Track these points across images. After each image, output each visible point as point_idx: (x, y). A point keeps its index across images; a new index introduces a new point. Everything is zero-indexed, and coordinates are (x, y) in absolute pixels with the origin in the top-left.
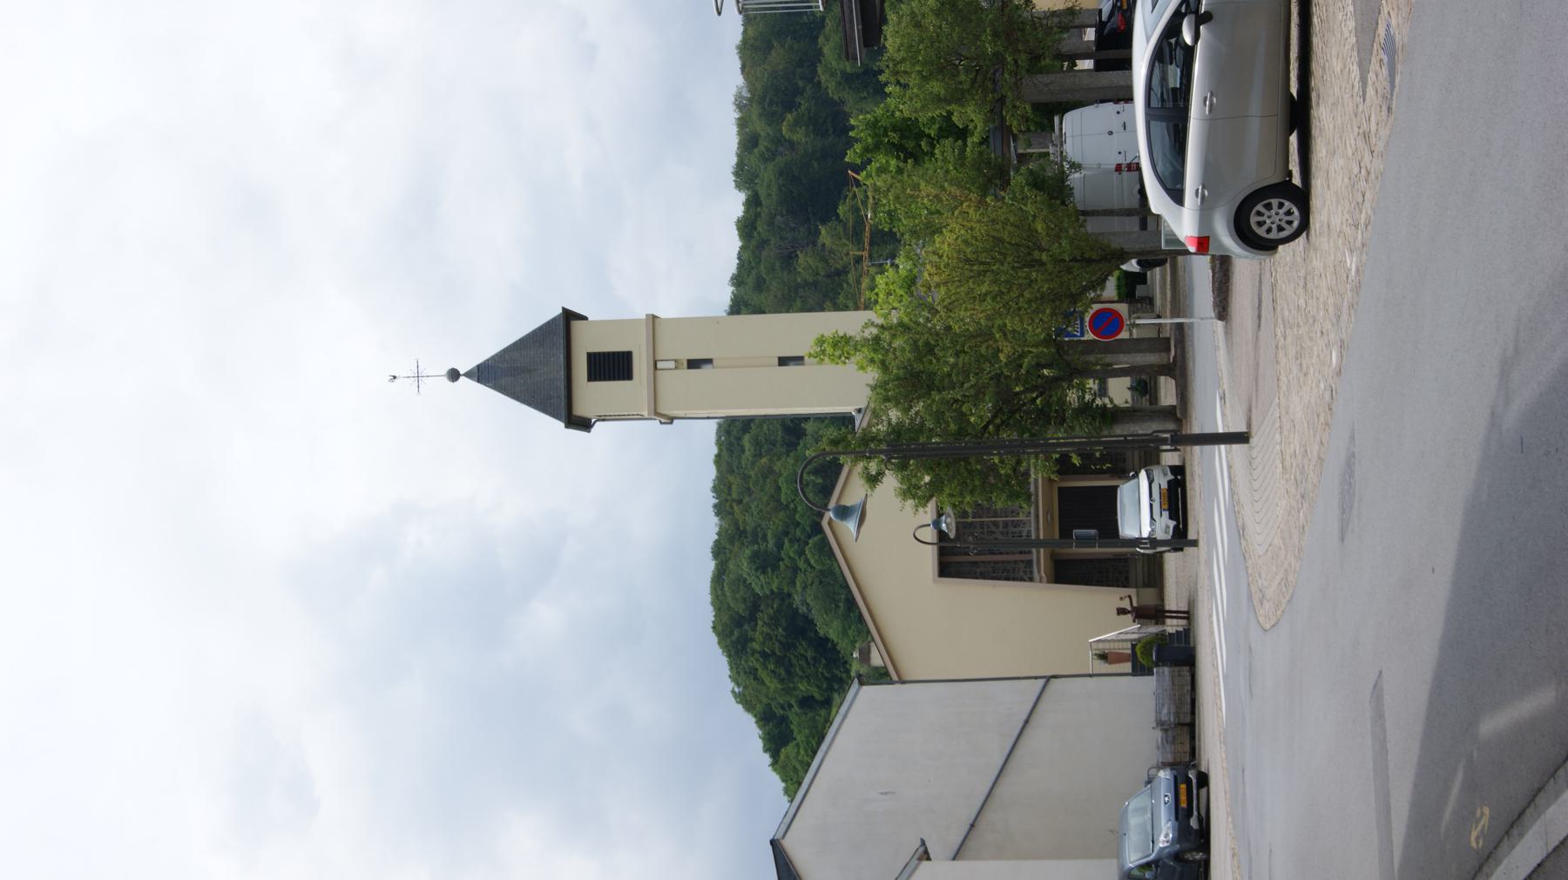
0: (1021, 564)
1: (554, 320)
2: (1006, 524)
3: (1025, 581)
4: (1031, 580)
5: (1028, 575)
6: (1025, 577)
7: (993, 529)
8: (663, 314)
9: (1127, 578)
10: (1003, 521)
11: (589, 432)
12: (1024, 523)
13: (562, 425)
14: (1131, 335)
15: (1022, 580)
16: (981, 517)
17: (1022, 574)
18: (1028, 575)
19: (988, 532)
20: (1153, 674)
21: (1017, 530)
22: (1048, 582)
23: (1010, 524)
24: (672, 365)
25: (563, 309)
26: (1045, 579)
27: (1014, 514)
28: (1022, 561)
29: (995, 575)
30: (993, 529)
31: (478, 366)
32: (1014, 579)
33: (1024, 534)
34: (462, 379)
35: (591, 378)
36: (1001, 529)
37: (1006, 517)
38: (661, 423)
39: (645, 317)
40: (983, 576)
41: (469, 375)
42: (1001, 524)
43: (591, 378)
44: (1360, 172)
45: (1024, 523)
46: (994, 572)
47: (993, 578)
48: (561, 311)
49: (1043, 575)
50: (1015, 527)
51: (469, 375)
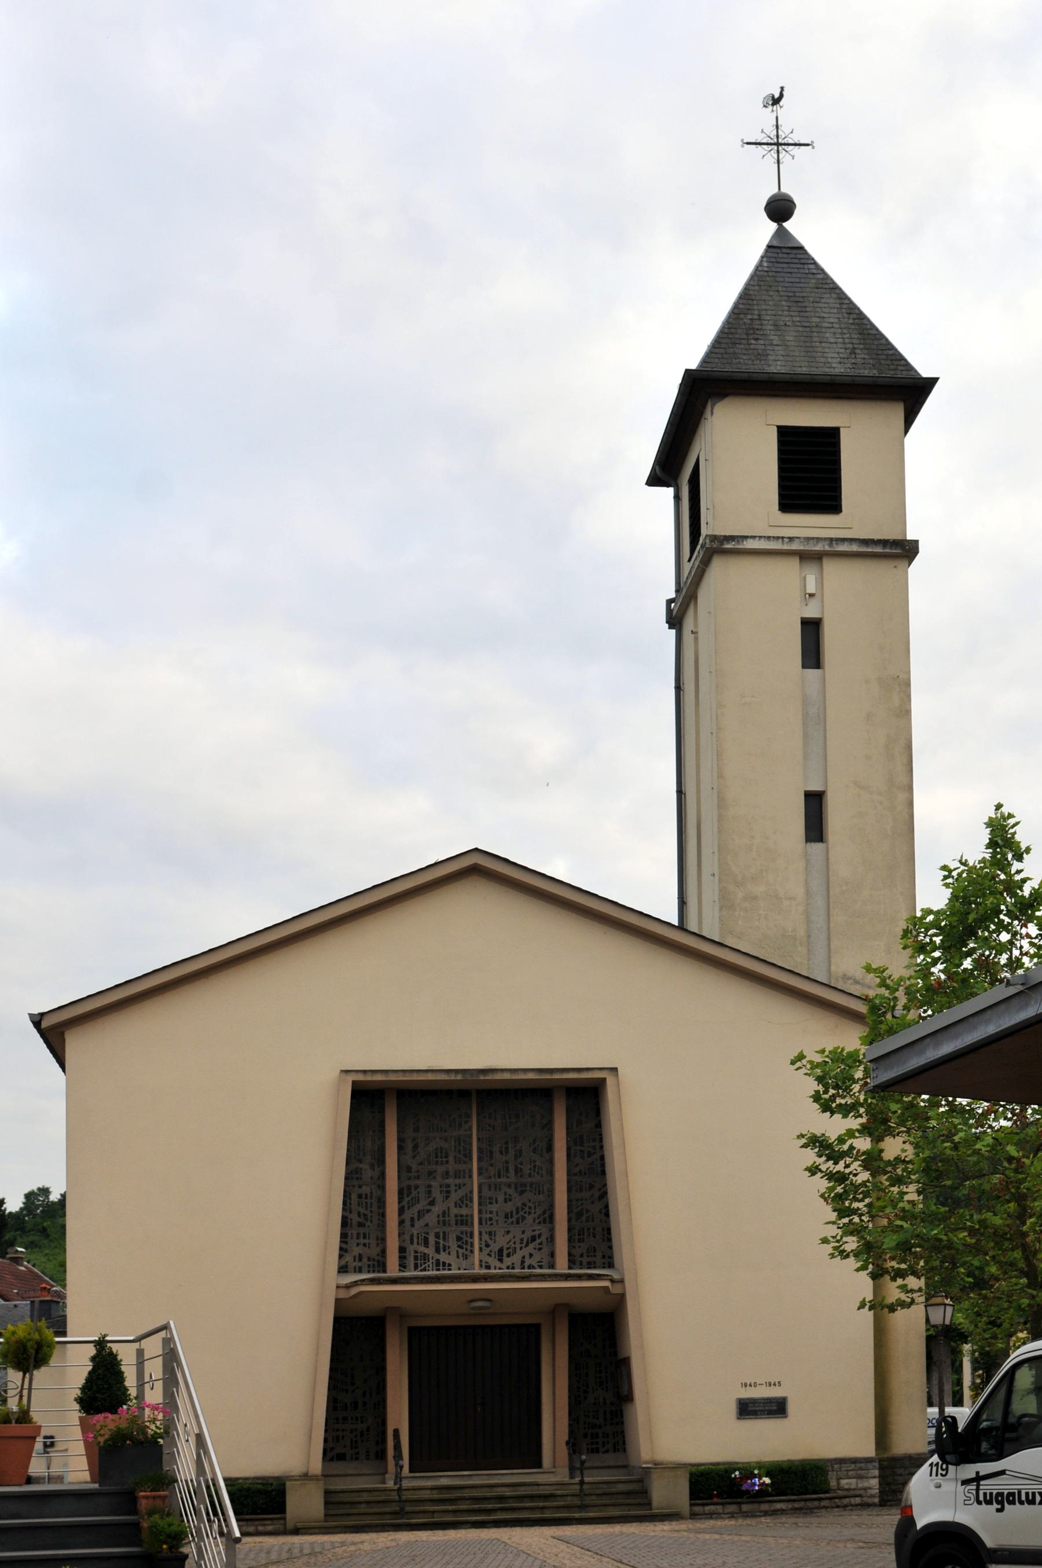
0: (378, 1250)
1: (898, 359)
2: (465, 1221)
3: (341, 1257)
4: (343, 1270)
5: (353, 1265)
6: (348, 1258)
7: (455, 1196)
8: (916, 569)
9: (341, 1457)
10: (472, 1216)
11: (686, 370)
12: (466, 1257)
13: (694, 366)
14: (874, 1477)
15: (343, 1251)
16: (480, 1174)
17: (356, 1251)
18: (353, 1265)
19: (448, 1186)
20: (922, 910)
21: (453, 1243)
22: (338, 1301)
23: (465, 1228)
24: (811, 588)
25: (933, 381)
26: (343, 1294)
27: (486, 1237)
28: (384, 1252)
29: (354, 1197)
30: (455, 1196)
31: (802, 248)
32: (344, 1236)
33: (443, 1257)
34: (773, 226)
35: (786, 434)
36: (454, 1211)
37: (480, 1223)
38: (669, 602)
39: (910, 536)
40: (352, 1176)
41: (782, 233)
42: (464, 1211)
43: (786, 434)
44: (617, 1536)
45: (466, 1257)
46: (360, 1196)
47: (347, 1195)
48: (925, 373)
49: (354, 1291)
50: (459, 1239)
51: (782, 233)
